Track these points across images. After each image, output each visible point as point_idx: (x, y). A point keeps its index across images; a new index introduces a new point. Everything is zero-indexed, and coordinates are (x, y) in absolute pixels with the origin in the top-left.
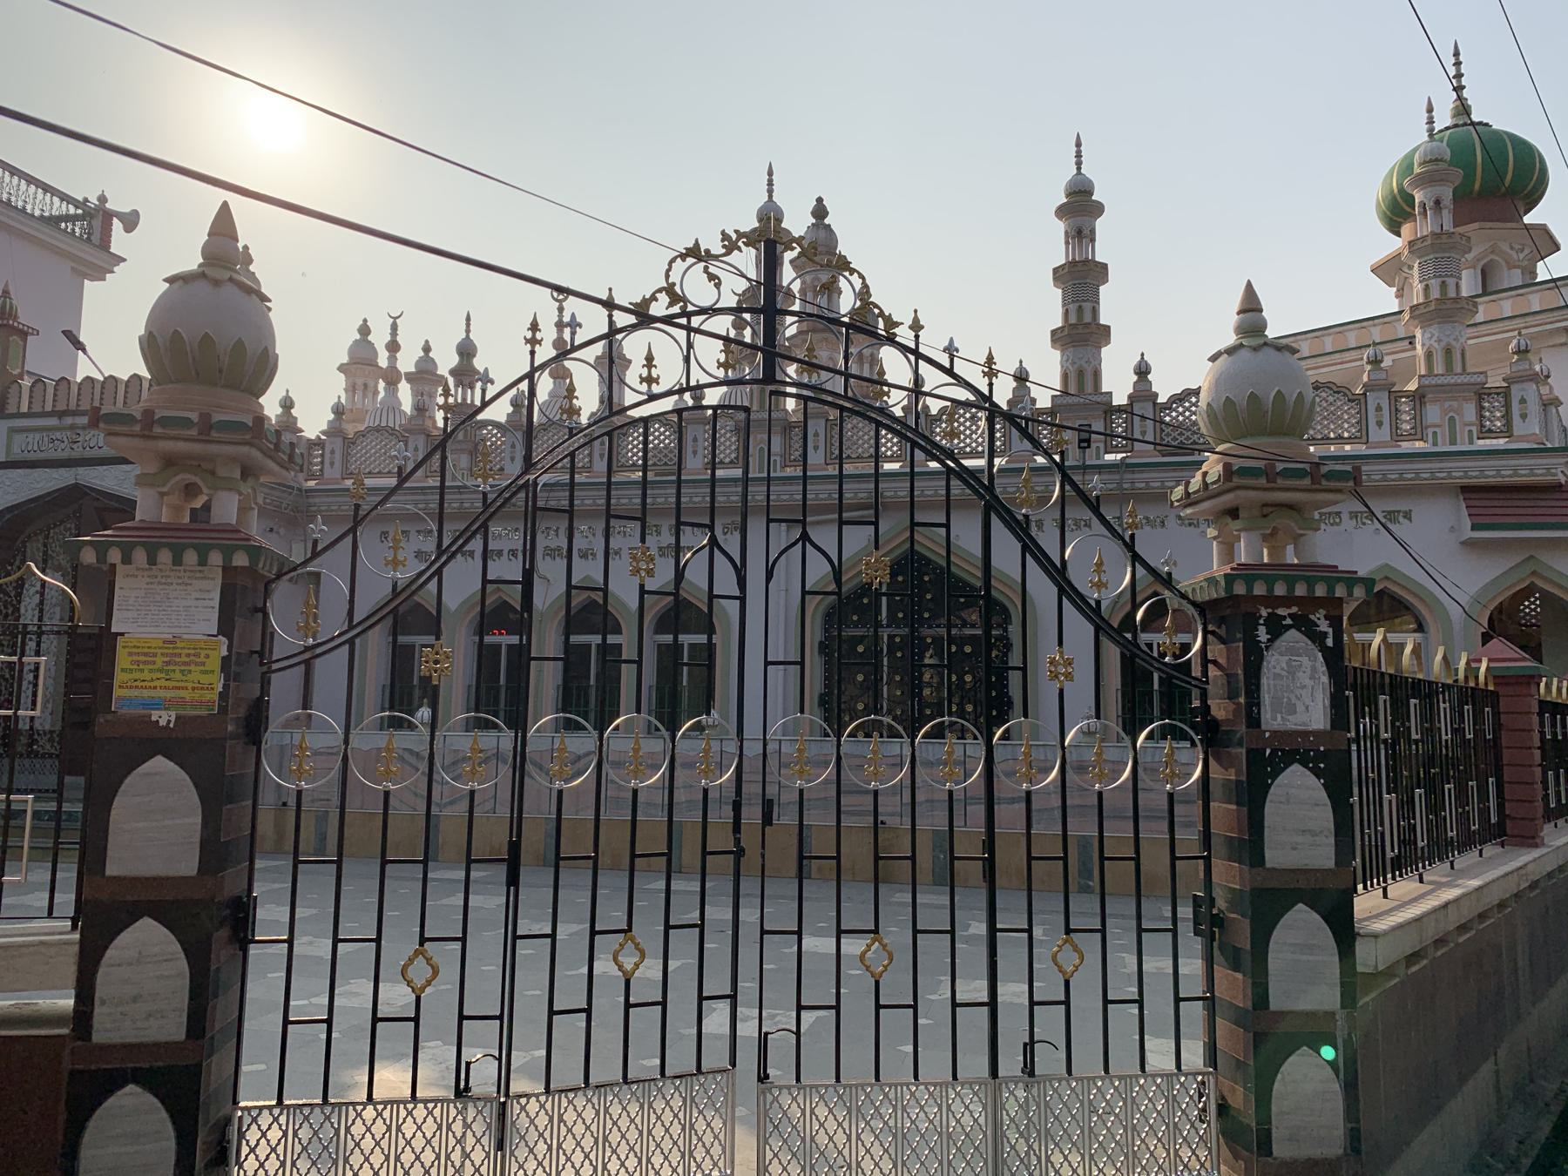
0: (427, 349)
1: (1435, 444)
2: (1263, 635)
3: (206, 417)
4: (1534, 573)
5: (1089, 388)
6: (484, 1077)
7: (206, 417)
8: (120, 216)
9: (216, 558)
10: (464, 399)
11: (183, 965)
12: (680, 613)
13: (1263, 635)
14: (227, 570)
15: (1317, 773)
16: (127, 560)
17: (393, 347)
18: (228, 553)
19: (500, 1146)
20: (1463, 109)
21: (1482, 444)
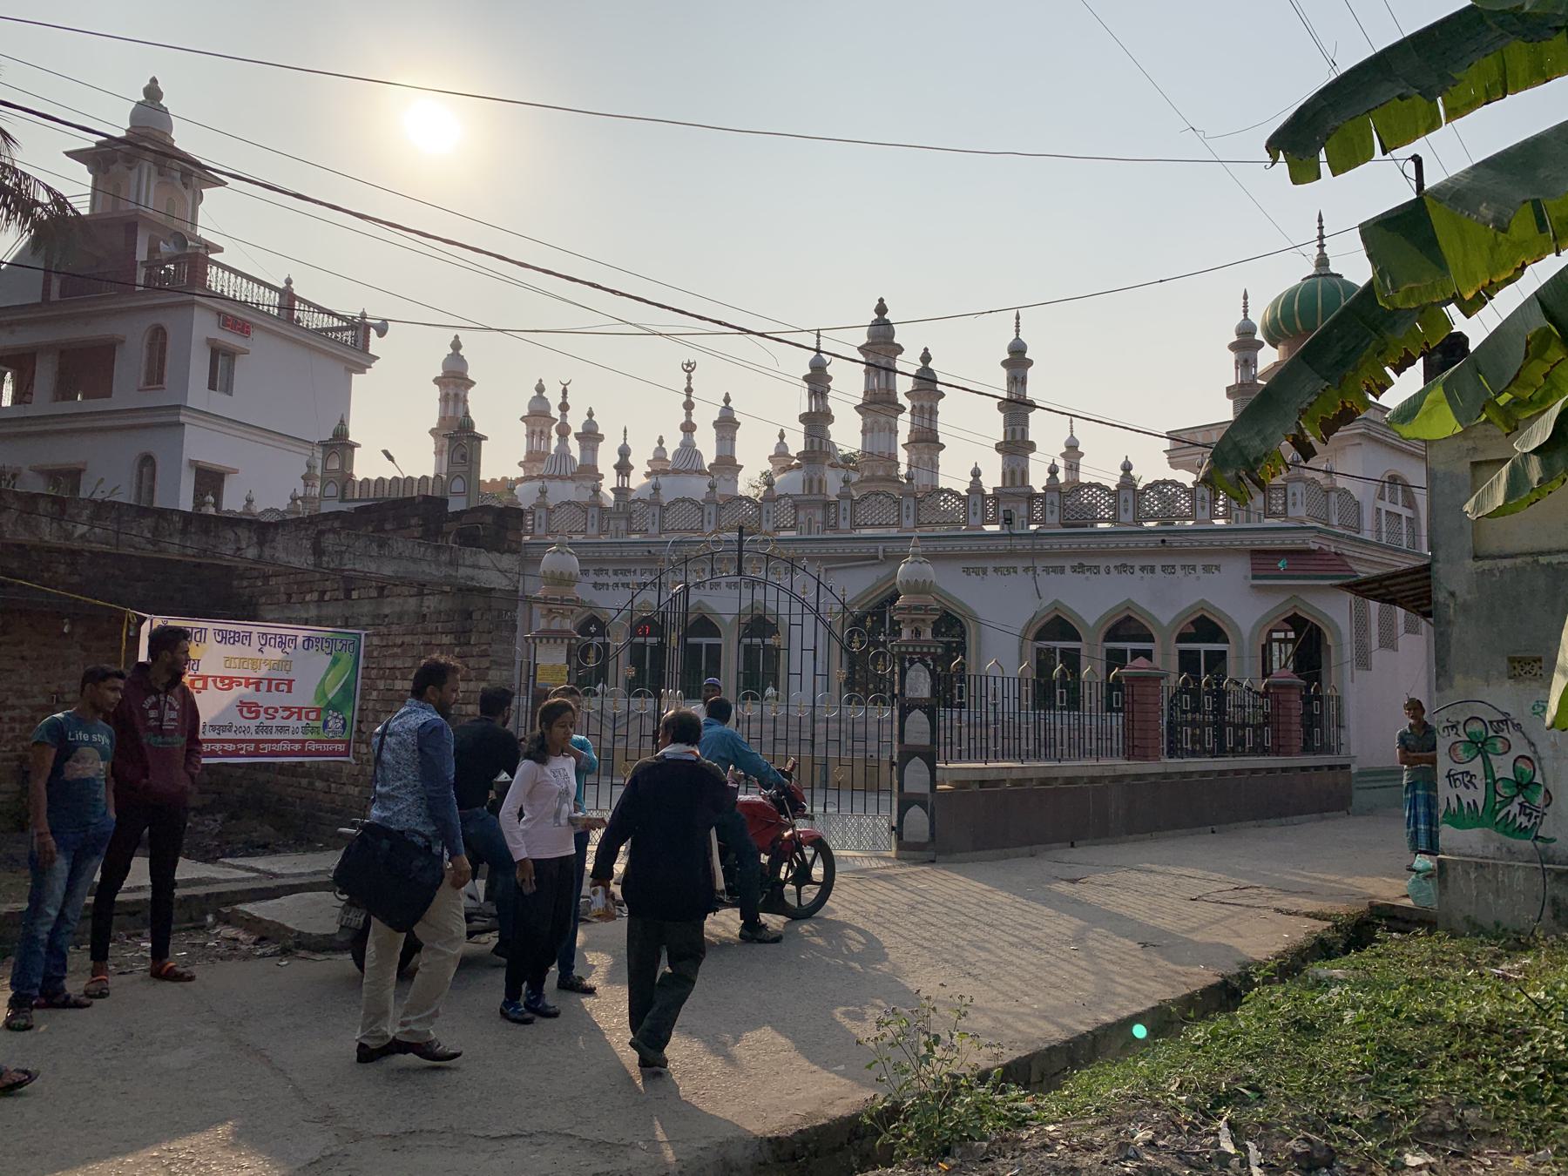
0: (590, 414)
8: (374, 326)
12: (759, 625)
17: (564, 407)
20: (1323, 261)
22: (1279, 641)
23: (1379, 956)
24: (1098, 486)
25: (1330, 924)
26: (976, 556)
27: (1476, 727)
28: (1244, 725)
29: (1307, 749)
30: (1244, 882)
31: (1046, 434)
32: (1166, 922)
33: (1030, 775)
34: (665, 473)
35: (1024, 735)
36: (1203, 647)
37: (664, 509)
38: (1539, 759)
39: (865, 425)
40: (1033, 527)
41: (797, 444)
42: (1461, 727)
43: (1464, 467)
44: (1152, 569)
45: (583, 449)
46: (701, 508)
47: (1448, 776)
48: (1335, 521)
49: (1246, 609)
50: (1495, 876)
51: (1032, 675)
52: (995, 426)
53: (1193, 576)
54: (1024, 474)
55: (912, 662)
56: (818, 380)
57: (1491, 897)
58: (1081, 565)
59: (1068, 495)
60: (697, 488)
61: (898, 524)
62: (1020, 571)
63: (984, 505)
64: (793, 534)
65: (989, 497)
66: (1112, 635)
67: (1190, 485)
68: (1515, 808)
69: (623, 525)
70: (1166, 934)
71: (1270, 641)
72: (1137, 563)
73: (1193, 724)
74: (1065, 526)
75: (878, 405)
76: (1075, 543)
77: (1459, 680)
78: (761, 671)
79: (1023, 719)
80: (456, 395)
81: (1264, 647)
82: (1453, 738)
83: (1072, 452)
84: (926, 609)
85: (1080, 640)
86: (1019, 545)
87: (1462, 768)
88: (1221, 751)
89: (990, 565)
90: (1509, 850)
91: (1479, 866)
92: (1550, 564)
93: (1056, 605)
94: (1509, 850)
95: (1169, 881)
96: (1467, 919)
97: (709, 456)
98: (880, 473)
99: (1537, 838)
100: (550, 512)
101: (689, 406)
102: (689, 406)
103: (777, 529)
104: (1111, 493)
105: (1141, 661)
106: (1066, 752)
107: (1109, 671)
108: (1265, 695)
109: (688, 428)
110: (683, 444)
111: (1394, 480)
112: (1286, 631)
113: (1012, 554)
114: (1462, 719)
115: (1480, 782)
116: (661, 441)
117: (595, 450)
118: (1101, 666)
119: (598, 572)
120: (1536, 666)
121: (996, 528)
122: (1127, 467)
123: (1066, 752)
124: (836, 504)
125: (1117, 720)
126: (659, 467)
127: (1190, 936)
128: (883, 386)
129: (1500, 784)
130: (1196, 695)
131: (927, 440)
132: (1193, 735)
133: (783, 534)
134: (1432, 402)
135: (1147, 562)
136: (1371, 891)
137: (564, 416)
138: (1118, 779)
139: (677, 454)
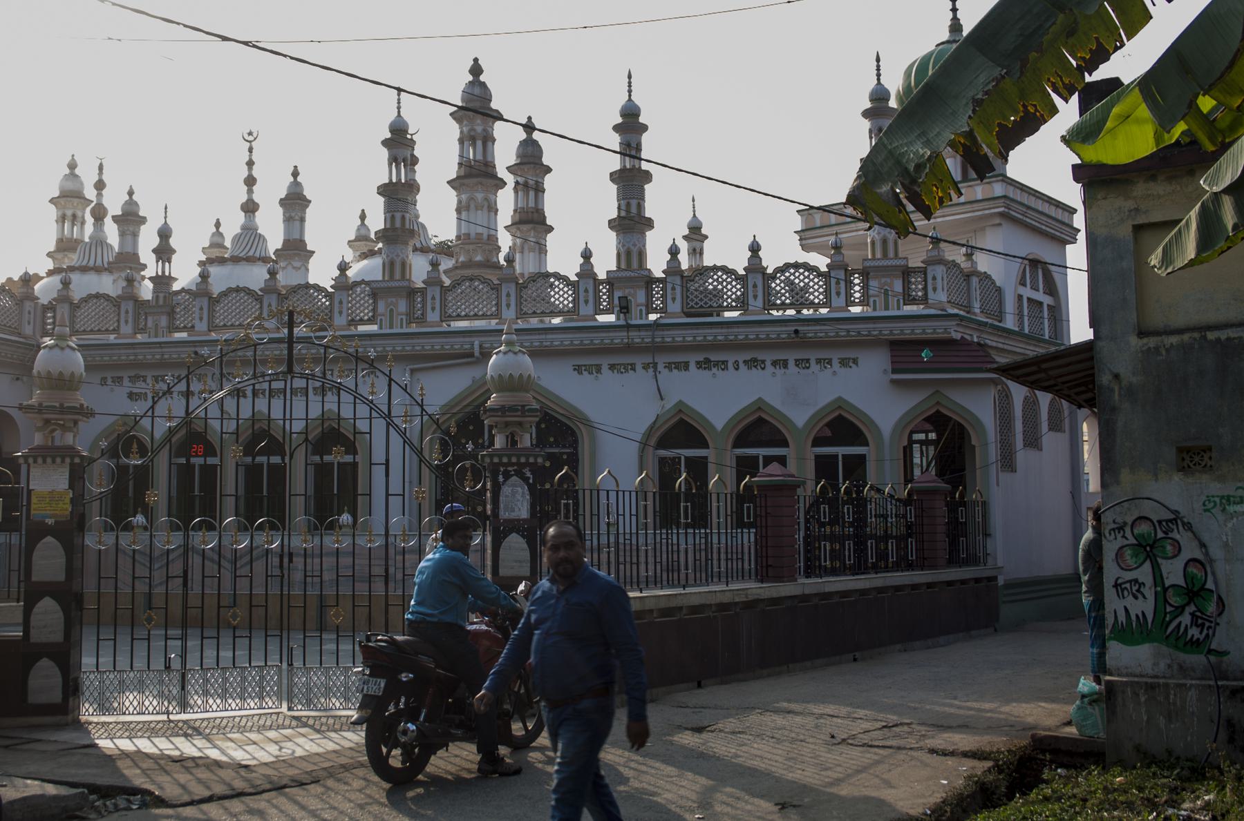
0: (131, 193)
1: (875, 309)
2: (501, 479)
3: (61, 405)
4: (938, 403)
5: (635, 265)
6: (176, 664)
7: (61, 405)
9: (68, 460)
10: (163, 272)
11: (61, 614)
13: (501, 479)
14: (72, 464)
15: (523, 536)
16: (35, 462)
17: (100, 185)
18: (72, 458)
19: (183, 688)
21: (909, 309)
22: (921, 442)
23: (1047, 799)
24: (724, 269)
25: (989, 764)
26: (589, 351)
27: (1143, 528)
28: (886, 537)
29: (953, 561)
30: (894, 718)
31: (666, 207)
32: (807, 775)
33: (649, 605)
34: (221, 261)
35: (642, 559)
36: (841, 451)
37: (214, 301)
38: (1211, 561)
39: (459, 202)
40: (653, 317)
41: (377, 222)
42: (1128, 530)
43: (1125, 231)
44: (785, 364)
45: (122, 234)
46: (259, 299)
47: (1116, 585)
48: (976, 306)
49: (884, 404)
50: (1167, 697)
51: (652, 488)
52: (608, 202)
53: (829, 371)
54: (642, 255)
55: (507, 476)
56: (399, 143)
57: (1162, 721)
58: (707, 361)
59: (691, 282)
60: (256, 277)
61: (497, 315)
62: (639, 367)
63: (597, 291)
64: (373, 328)
65: (602, 282)
66: (740, 441)
67: (824, 269)
68: (1186, 619)
69: (164, 321)
70: (805, 789)
71: (911, 442)
72: (769, 357)
73: (832, 538)
74: (688, 315)
75: (475, 176)
76: (701, 335)
77: (1125, 476)
78: (337, 494)
79: (642, 540)
80: (74, 216)
81: (905, 448)
82: (1120, 542)
83: (695, 233)
84: (523, 410)
85: (706, 446)
86: (637, 337)
87: (1129, 576)
88: (860, 568)
89: (605, 362)
90: (1181, 667)
91: (1151, 687)
92: (1218, 340)
93: (681, 408)
94: (1181, 667)
95: (809, 721)
96: (1138, 748)
97: (274, 239)
98: (479, 258)
99: (1210, 651)
100: (74, 307)
101: (250, 181)
102: (250, 181)
103: (353, 322)
104: (739, 278)
105: (774, 468)
106: (691, 576)
107: (740, 479)
108: (907, 502)
109: (250, 208)
110: (244, 228)
111: (1035, 263)
112: (926, 432)
113: (629, 348)
114: (1129, 520)
115: (1149, 592)
116: (218, 225)
117: (135, 235)
118: (730, 475)
119: (134, 379)
120: (1206, 457)
121: (611, 318)
122: (755, 248)
123: (691, 576)
124: (423, 292)
125: (748, 537)
126: (215, 257)
127: (834, 790)
128: (479, 157)
129: (1170, 592)
130: (834, 503)
131: (532, 222)
132: (832, 550)
133: (362, 328)
134: (1119, 116)
135: (780, 355)
136: (1030, 720)
137: (99, 195)
138: (751, 605)
139: (237, 239)
